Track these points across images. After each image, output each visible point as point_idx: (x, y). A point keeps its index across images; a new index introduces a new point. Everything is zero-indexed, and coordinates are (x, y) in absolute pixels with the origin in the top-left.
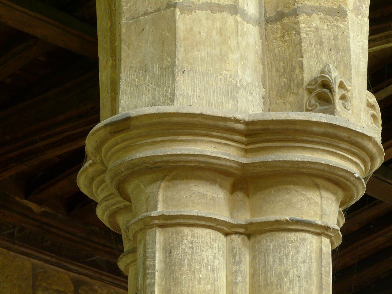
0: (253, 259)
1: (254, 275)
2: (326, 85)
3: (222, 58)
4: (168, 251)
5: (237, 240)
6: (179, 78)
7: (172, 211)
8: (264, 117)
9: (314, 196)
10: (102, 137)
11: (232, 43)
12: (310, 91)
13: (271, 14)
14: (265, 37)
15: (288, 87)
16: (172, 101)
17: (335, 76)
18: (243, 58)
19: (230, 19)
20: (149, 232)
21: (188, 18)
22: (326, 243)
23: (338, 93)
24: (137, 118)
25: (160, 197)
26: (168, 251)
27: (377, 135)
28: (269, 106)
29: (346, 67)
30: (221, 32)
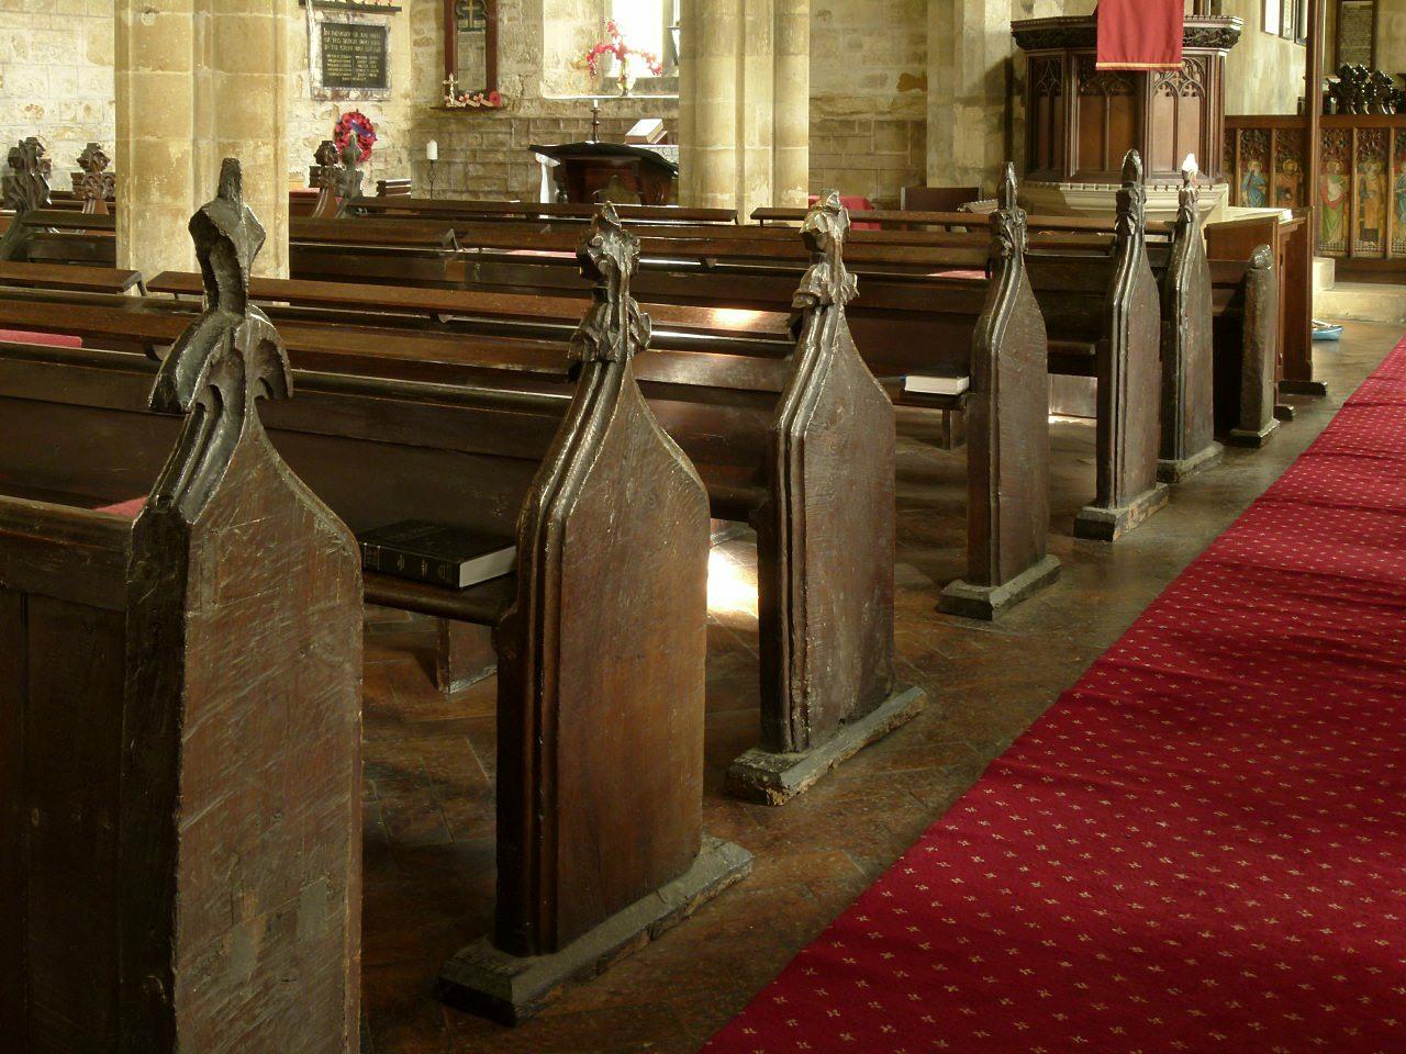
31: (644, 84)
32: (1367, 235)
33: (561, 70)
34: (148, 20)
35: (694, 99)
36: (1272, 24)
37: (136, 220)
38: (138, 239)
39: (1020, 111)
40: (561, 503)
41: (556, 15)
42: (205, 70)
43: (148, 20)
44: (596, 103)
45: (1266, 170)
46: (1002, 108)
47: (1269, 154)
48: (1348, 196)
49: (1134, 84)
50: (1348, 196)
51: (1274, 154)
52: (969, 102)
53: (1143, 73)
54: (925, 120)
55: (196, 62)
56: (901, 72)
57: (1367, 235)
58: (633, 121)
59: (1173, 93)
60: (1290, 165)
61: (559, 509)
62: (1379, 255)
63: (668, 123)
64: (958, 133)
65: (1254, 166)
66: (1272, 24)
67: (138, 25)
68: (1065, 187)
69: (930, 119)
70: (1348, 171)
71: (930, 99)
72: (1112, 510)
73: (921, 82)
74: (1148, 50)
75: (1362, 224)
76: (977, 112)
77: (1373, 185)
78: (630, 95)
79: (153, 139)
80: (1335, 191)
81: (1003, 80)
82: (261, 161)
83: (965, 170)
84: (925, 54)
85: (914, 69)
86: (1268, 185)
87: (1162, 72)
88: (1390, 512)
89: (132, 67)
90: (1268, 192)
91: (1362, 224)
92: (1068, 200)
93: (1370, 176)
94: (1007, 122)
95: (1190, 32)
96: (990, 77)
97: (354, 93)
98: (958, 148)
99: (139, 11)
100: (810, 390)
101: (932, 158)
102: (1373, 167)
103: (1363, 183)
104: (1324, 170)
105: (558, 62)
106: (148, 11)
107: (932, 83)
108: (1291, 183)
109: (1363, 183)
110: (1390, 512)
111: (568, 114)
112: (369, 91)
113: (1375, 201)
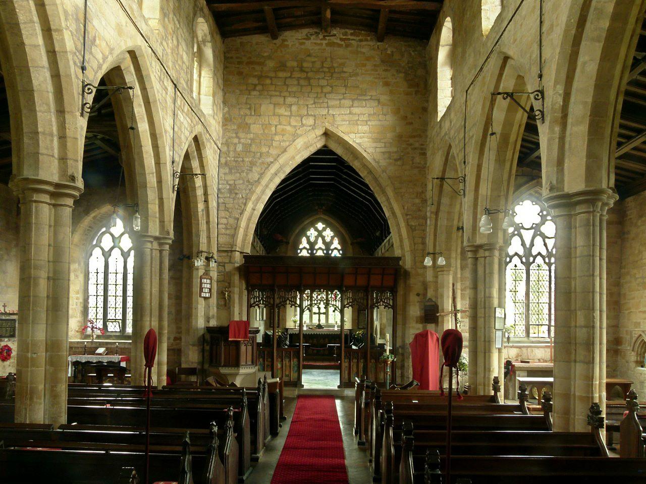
0: (55, 212)
1: (55, 215)
2: (73, 177)
3: (50, 167)
4: (36, 207)
5: (51, 206)
6: (40, 170)
7: (37, 199)
8: (123, 101)
9: (69, 199)
10: (183, 366)
11: (52, 164)
12: (70, 177)
13: (61, 158)
14: (59, 163)
15: (64, 175)
16: (38, 176)
17: (75, 175)
18: (55, 167)
19: (52, 158)
20: (419, 163)
21: (42, 156)
22: (548, 350)
23: (76, 179)
24: (30, 179)
25: (34, 196)
26: (36, 207)
27: (83, 188)
28: (60, 180)
29: (78, 173)
30: (50, 161)
31: (98, 337)
32: (287, 376)
33: (73, 333)
34: (35, 356)
35: (136, 353)
36: (258, 319)
37: (29, 406)
38: (30, 411)
39: (207, 348)
40: (210, 476)
41: (72, 317)
42: (48, 367)
43: (35, 356)
44: (86, 343)
45: (264, 361)
46: (202, 347)
47: (264, 357)
48: (282, 367)
49: (237, 344)
50: (282, 367)
51: (266, 357)
52: (193, 345)
53: (239, 341)
54: (181, 349)
55: (45, 365)
56: (175, 336)
57: (287, 376)
58: (97, 348)
59: (246, 345)
60: (269, 360)
61: (211, 477)
62: (289, 380)
63: (107, 349)
64: (191, 353)
65: (261, 360)
66: (258, 319)
67: (32, 358)
68: (220, 368)
69: (182, 349)
70: (282, 361)
71: (183, 344)
72: (258, 455)
73: (180, 339)
74: (240, 336)
75: (285, 374)
76: (196, 348)
77: (288, 364)
78: (95, 340)
79: (35, 386)
80: (279, 366)
81: (202, 340)
82: (63, 389)
83: (192, 363)
84: (181, 332)
85: (177, 335)
86: (264, 364)
87: (244, 341)
88: (309, 449)
89: (29, 367)
90: (264, 367)
91: (285, 374)
92: (221, 371)
93: (287, 362)
94: (203, 351)
95: (250, 331)
96: (199, 339)
97: (6, 340)
98: (190, 356)
99: (32, 353)
100: (229, 445)
101: (183, 359)
102: (287, 360)
103: (286, 363)
104: (277, 361)
105: (72, 330)
106: (35, 353)
107: (183, 340)
108: (270, 364)
109: (286, 363)
110: (309, 449)
111: (76, 346)
112: (10, 338)
113: (288, 368)
